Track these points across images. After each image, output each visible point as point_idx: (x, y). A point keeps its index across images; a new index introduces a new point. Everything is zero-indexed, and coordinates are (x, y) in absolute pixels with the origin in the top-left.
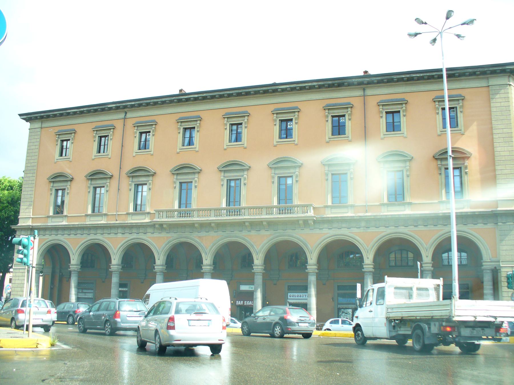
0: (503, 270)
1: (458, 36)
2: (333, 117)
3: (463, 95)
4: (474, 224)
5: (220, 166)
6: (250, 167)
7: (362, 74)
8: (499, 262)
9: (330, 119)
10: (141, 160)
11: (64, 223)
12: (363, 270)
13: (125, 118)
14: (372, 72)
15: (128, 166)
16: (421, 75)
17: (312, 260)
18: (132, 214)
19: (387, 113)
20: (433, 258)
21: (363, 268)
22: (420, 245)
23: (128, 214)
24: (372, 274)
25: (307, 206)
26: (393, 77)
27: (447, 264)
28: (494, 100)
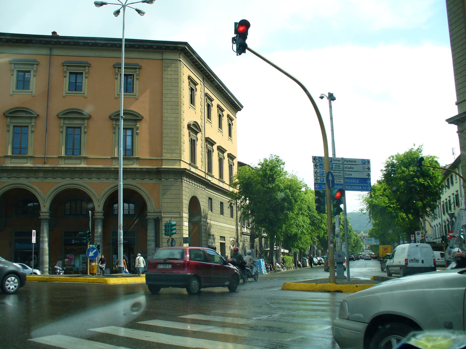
0: (164, 220)
1: (139, 11)
2: (18, 71)
3: (90, 63)
4: (142, 179)
5: (112, 115)
6: (38, 115)
7: (51, 34)
8: (161, 212)
9: (15, 73)
10: (74, 102)
11: (83, 165)
12: (40, 217)
13: (50, 55)
14: (60, 34)
16: (105, 42)
19: (71, 73)
20: (104, 208)
21: (40, 216)
22: (93, 196)
24: (48, 221)
26: (79, 41)
27: (128, 213)
28: (166, 72)
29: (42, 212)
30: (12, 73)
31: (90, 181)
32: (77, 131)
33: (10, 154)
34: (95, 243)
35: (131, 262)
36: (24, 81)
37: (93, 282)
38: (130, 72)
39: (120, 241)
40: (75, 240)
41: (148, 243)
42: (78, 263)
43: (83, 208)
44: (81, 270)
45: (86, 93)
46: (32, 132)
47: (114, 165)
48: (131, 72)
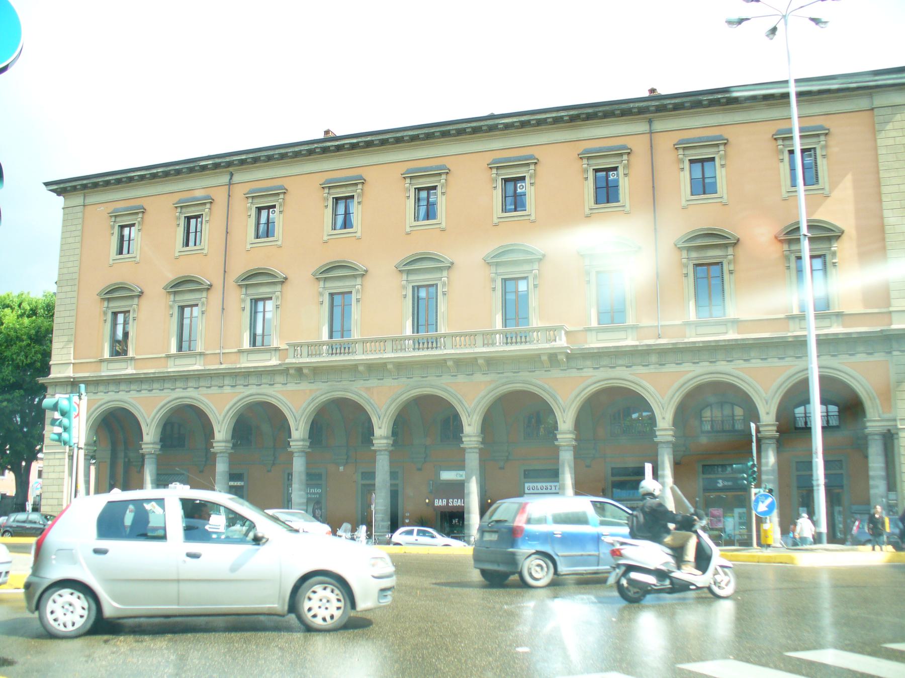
1: (816, 21)
3: (726, 136)
4: (851, 355)
5: (399, 264)
6: (452, 263)
8: (895, 420)
9: (591, 175)
13: (651, 133)
15: (239, 268)
17: (566, 422)
18: (248, 352)
20: (675, 423)
21: (656, 436)
23: (241, 352)
24: (774, 441)
25: (554, 329)
26: (700, 98)
27: (803, 425)
28: (883, 134)
29: (659, 430)
30: (781, 157)
31: (747, 365)
32: (715, 270)
33: (594, 324)
34: (763, 486)
35: (837, 522)
36: (607, 187)
37: (769, 560)
38: (810, 143)
39: (817, 480)
40: (724, 479)
41: (871, 482)
42: (730, 524)
43: (736, 418)
44: (737, 538)
45: (725, 196)
46: (358, 300)
47: (793, 331)
48: (198, 211)
